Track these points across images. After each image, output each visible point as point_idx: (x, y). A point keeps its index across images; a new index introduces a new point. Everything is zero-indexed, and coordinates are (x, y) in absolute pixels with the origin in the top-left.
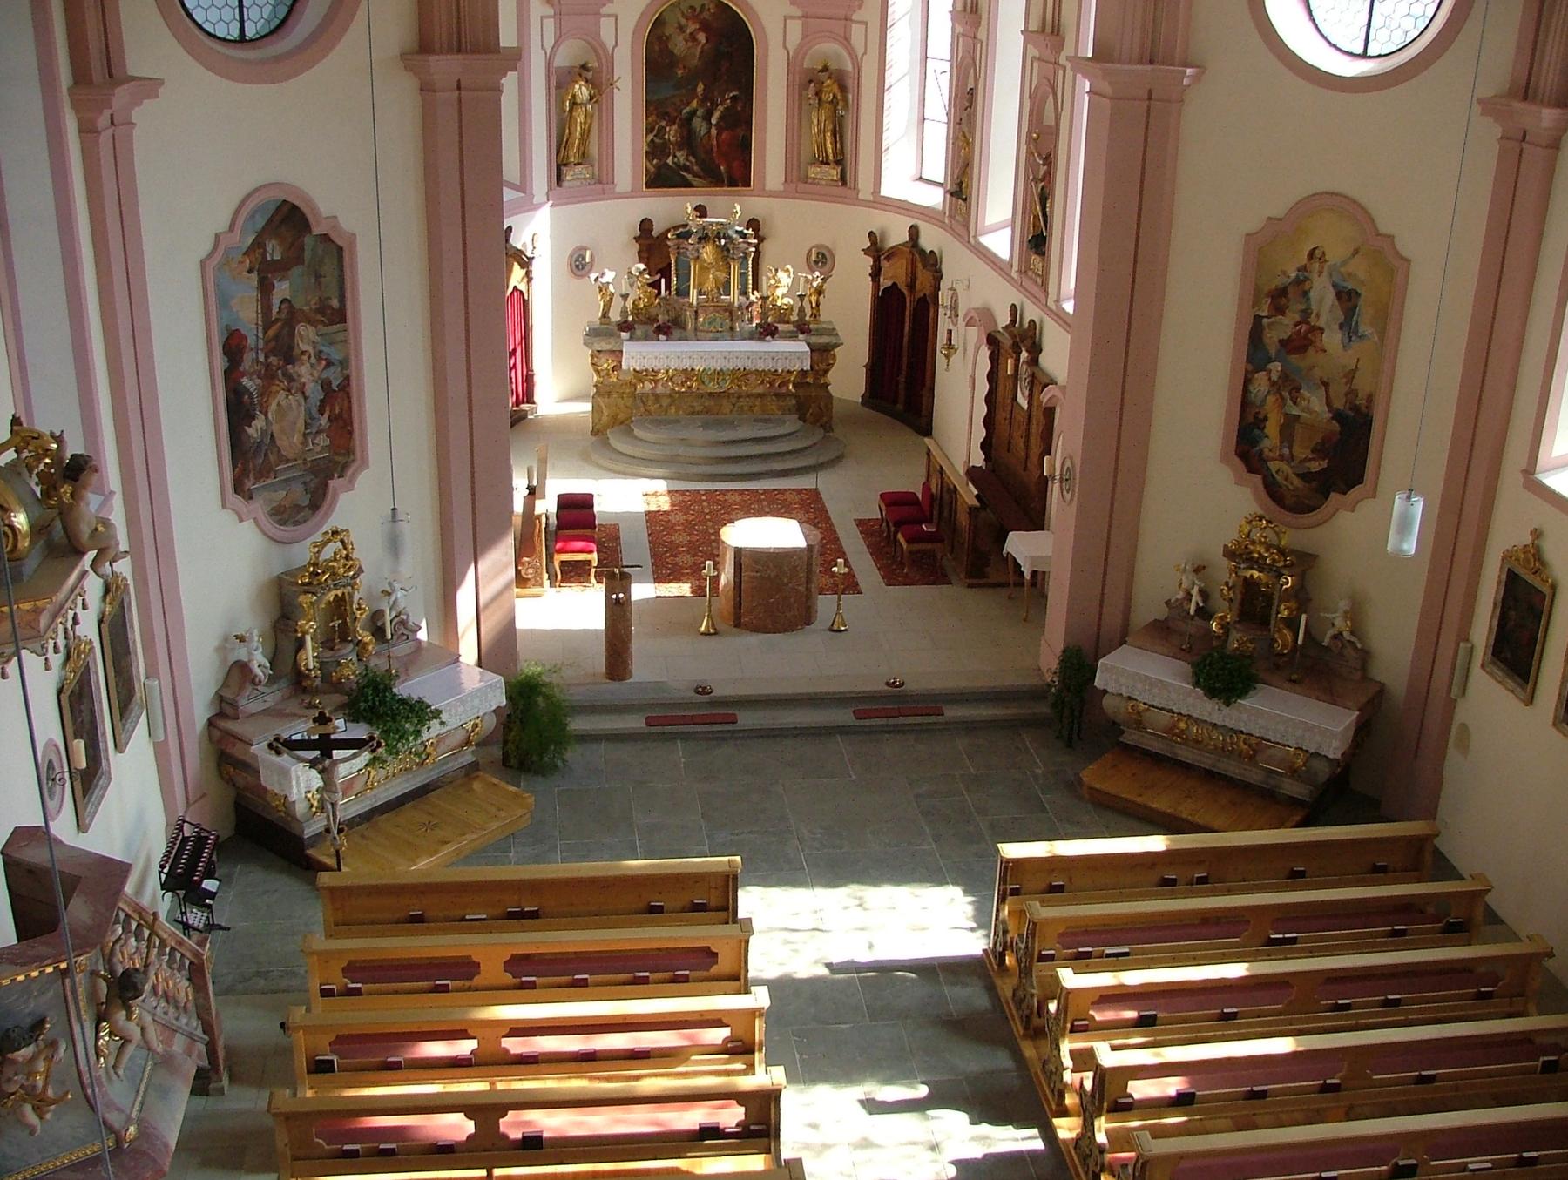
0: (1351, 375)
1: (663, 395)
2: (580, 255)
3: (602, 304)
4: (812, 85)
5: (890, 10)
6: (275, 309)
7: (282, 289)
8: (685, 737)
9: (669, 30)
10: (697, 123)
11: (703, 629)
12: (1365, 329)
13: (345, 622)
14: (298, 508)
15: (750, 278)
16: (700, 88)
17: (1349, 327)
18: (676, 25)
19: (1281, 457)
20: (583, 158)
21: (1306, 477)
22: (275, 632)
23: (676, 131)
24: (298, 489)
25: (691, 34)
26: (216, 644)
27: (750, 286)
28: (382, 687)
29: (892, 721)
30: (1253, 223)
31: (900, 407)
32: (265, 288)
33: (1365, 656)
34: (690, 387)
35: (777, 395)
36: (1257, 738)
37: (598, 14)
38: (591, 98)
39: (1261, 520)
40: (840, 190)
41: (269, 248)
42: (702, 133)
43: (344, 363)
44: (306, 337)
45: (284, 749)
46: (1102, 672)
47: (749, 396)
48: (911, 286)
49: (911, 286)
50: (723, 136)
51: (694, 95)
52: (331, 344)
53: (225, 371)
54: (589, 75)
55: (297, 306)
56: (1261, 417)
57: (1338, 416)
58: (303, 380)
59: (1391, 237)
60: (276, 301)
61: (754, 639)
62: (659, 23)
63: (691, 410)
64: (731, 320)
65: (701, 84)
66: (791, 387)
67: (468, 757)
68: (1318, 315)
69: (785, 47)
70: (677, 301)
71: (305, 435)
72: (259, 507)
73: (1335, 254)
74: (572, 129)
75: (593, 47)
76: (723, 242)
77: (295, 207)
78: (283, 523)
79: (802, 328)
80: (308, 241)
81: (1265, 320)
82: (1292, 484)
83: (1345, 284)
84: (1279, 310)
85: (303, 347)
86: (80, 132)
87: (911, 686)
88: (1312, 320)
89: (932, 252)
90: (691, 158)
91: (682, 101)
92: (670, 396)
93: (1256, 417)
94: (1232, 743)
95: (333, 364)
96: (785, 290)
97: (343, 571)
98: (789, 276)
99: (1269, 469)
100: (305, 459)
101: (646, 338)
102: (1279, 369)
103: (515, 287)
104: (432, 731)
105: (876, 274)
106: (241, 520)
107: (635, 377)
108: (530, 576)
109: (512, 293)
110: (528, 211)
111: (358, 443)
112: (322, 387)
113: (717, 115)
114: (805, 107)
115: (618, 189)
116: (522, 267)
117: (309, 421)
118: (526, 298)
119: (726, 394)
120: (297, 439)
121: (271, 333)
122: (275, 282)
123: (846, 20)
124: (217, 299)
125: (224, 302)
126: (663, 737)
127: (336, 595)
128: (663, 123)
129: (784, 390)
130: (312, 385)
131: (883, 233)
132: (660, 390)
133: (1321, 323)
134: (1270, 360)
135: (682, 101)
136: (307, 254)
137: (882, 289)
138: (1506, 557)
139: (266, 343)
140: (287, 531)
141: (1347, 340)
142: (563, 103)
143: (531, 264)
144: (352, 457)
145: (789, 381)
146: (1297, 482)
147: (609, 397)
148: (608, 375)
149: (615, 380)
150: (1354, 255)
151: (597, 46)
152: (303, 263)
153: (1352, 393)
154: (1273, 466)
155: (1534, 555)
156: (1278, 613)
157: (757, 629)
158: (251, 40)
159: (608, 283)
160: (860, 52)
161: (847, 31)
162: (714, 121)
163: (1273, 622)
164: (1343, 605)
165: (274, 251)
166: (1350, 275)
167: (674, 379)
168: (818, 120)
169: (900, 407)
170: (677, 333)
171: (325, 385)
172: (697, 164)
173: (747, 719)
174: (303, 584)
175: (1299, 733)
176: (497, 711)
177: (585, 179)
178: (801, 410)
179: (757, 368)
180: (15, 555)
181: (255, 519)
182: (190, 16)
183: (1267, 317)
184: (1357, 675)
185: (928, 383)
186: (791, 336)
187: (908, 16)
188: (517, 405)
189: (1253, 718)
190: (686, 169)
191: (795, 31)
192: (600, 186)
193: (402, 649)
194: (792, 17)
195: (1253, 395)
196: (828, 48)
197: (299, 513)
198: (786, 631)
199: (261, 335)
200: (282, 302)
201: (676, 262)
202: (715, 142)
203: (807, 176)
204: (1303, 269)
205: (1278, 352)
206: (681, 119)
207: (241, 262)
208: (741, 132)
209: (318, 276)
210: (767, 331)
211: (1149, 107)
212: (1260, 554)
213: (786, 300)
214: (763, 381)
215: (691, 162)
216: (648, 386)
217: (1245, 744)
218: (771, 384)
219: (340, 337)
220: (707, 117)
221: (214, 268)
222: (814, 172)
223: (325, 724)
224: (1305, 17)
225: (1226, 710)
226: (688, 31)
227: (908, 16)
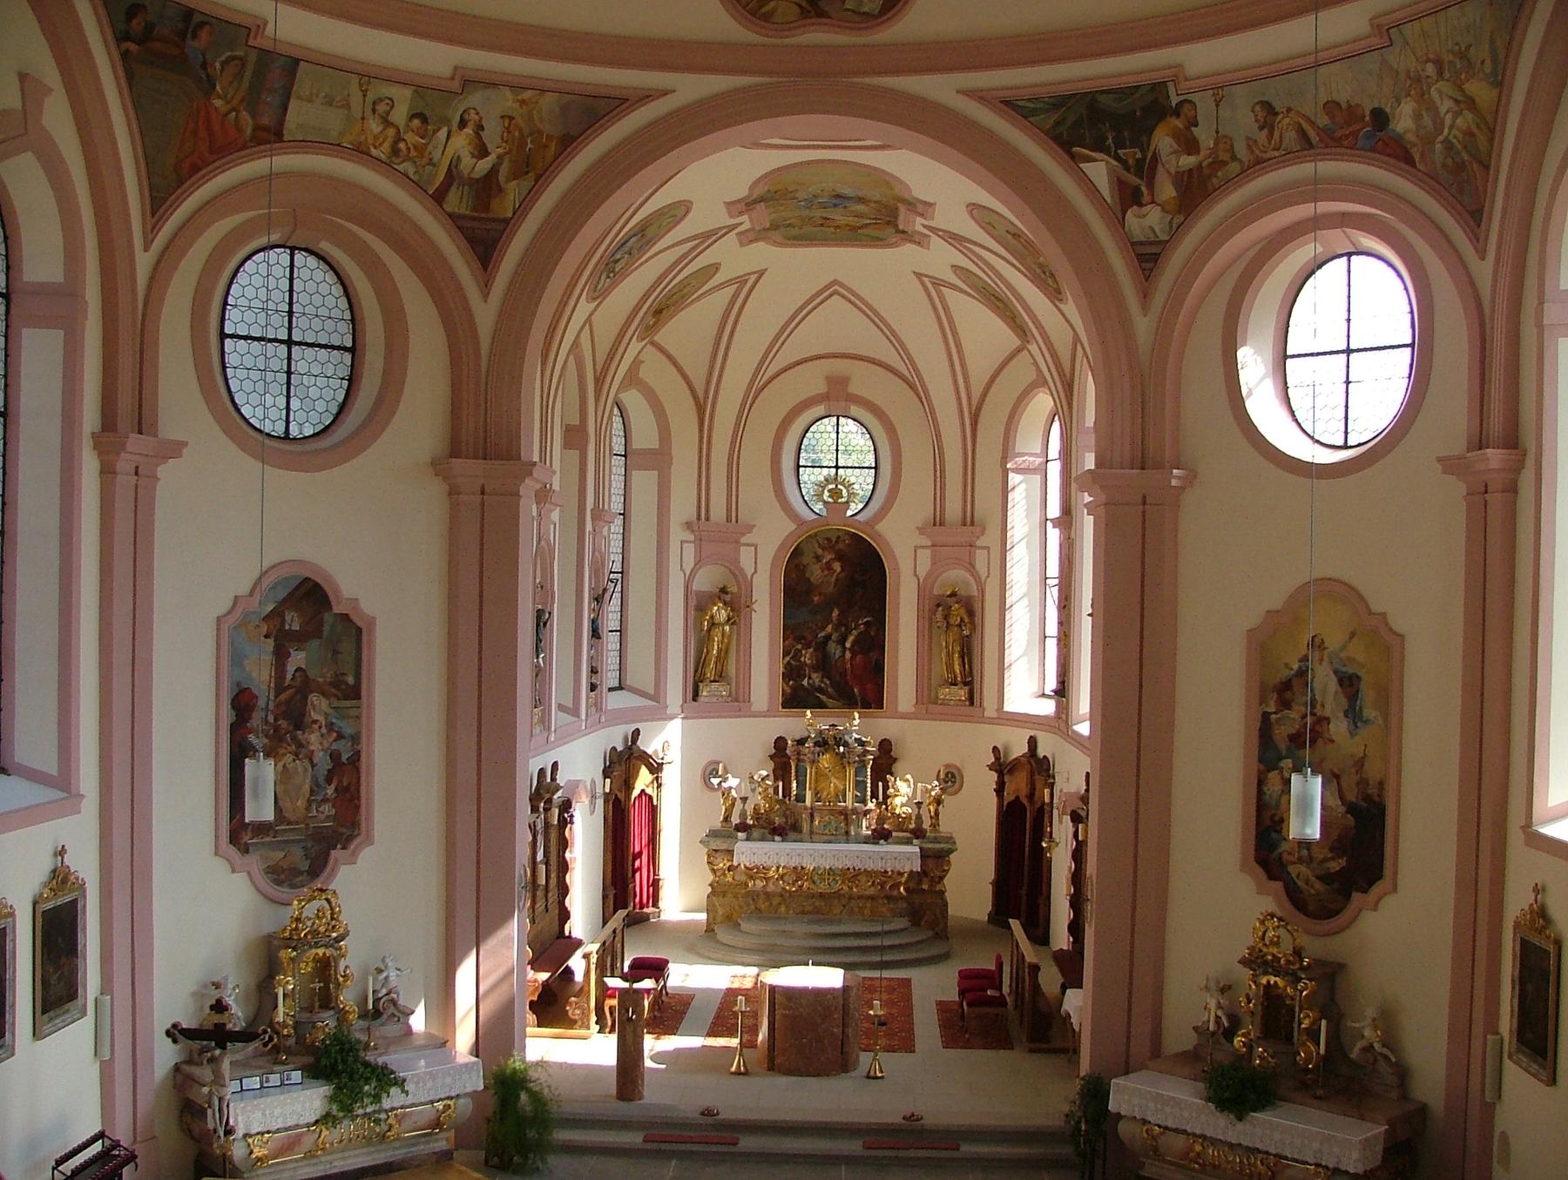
0: (1360, 764)
1: (774, 894)
2: (714, 769)
3: (724, 807)
4: (940, 609)
5: (1009, 534)
6: (289, 676)
7: (297, 659)
8: (681, 1155)
9: (807, 559)
10: (833, 648)
11: (733, 1069)
12: (1369, 713)
13: (327, 988)
14: (295, 872)
15: (869, 785)
16: (835, 613)
17: (1354, 714)
18: (812, 555)
19: (1301, 860)
20: (720, 677)
21: (1325, 878)
22: (260, 992)
24: (298, 852)
26: (194, 988)
27: (869, 793)
28: (347, 1046)
29: (901, 1153)
30: (1253, 619)
32: (281, 655)
33: (1403, 1074)
34: (801, 887)
35: (888, 898)
36: (1275, 1156)
38: (729, 620)
39: (1272, 918)
40: (968, 710)
41: (288, 618)
42: (837, 656)
43: (356, 739)
44: (319, 706)
45: (181, 1037)
46: (1115, 1093)
47: (860, 897)
48: (1031, 796)
49: (1031, 796)
50: (858, 659)
51: (828, 621)
52: (344, 717)
53: (231, 725)
54: (728, 598)
55: (311, 674)
56: (1277, 818)
57: (1351, 809)
58: (312, 748)
59: (1384, 615)
60: (291, 669)
61: (783, 1081)
62: (797, 553)
64: (847, 825)
66: (902, 889)
67: (441, 1143)
68: (1323, 706)
69: (916, 575)
70: (795, 806)
71: (309, 802)
72: (254, 861)
73: (1334, 640)
74: (710, 648)
75: (734, 574)
76: (842, 749)
77: (317, 585)
78: (279, 883)
79: (918, 833)
80: (328, 617)
81: (1273, 716)
82: (1312, 887)
83: (1344, 669)
84: (1285, 704)
85: (314, 716)
86: (101, 472)
87: (929, 1121)
88: (1318, 711)
89: (1045, 757)
90: (825, 680)
93: (1272, 818)
94: (1249, 1164)
95: (344, 737)
96: (905, 799)
97: (331, 936)
98: (909, 786)
99: (1289, 874)
100: (307, 824)
101: (763, 839)
102: (1291, 766)
103: (643, 791)
104: (393, 1099)
105: (1000, 791)
106: (233, 871)
107: (747, 874)
108: (577, 1017)
109: (640, 796)
110: (659, 719)
111: (363, 818)
112: (331, 758)
113: (851, 638)
114: (935, 630)
116: (651, 772)
117: (315, 788)
118: (655, 803)
120: (301, 803)
121: (283, 697)
122: (291, 650)
123: (971, 546)
124: (231, 654)
125: (237, 659)
126: (659, 1154)
127: (317, 954)
128: (799, 646)
129: (895, 893)
130: (321, 754)
131: (1006, 748)
132: (771, 887)
133: (1327, 713)
134: (1281, 758)
136: (327, 628)
137: (1005, 803)
138: (1517, 926)
139: (277, 706)
140: (282, 892)
141: (1353, 727)
142: (702, 623)
143: (661, 770)
144: (356, 833)
145: (899, 884)
146: (1318, 885)
147: (724, 896)
148: (724, 874)
149: (731, 880)
150: (1351, 638)
151: (737, 572)
152: (321, 638)
153: (1363, 783)
154: (1293, 870)
155: (1540, 916)
156: (1300, 1024)
157: (789, 1072)
158: (295, 439)
159: (730, 788)
160: (983, 574)
161: (971, 556)
162: (848, 645)
163: (1296, 1034)
164: (1370, 1012)
165: (293, 621)
166: (1349, 659)
167: (785, 878)
168: (946, 642)
170: (792, 835)
171: (335, 756)
172: (832, 687)
173: (748, 1143)
174: (285, 938)
175: (1316, 1145)
176: (474, 1095)
177: (722, 696)
178: (915, 916)
180: (228, 1128)
181: (249, 873)
182: (238, 410)
183: (1275, 713)
184: (1394, 1094)
186: (908, 842)
187: (1026, 540)
188: (641, 908)
189: (1268, 1132)
190: (820, 690)
191: (925, 557)
192: (736, 704)
193: (391, 1030)
195: (1267, 797)
196: (955, 576)
197: (297, 877)
198: (818, 1075)
199: (272, 697)
200: (296, 671)
201: (797, 766)
204: (1305, 659)
205: (1288, 749)
207: (258, 626)
208: (874, 655)
209: (336, 652)
210: (880, 835)
211: (1144, 512)
212: (1273, 955)
213: (904, 809)
214: (874, 882)
216: (760, 884)
217: (1262, 1164)
218: (882, 885)
219: (353, 712)
220: (842, 641)
221: (232, 629)
222: (945, 692)
223: (222, 1012)
224: (1288, 419)
225: (1240, 1126)
227: (1026, 540)
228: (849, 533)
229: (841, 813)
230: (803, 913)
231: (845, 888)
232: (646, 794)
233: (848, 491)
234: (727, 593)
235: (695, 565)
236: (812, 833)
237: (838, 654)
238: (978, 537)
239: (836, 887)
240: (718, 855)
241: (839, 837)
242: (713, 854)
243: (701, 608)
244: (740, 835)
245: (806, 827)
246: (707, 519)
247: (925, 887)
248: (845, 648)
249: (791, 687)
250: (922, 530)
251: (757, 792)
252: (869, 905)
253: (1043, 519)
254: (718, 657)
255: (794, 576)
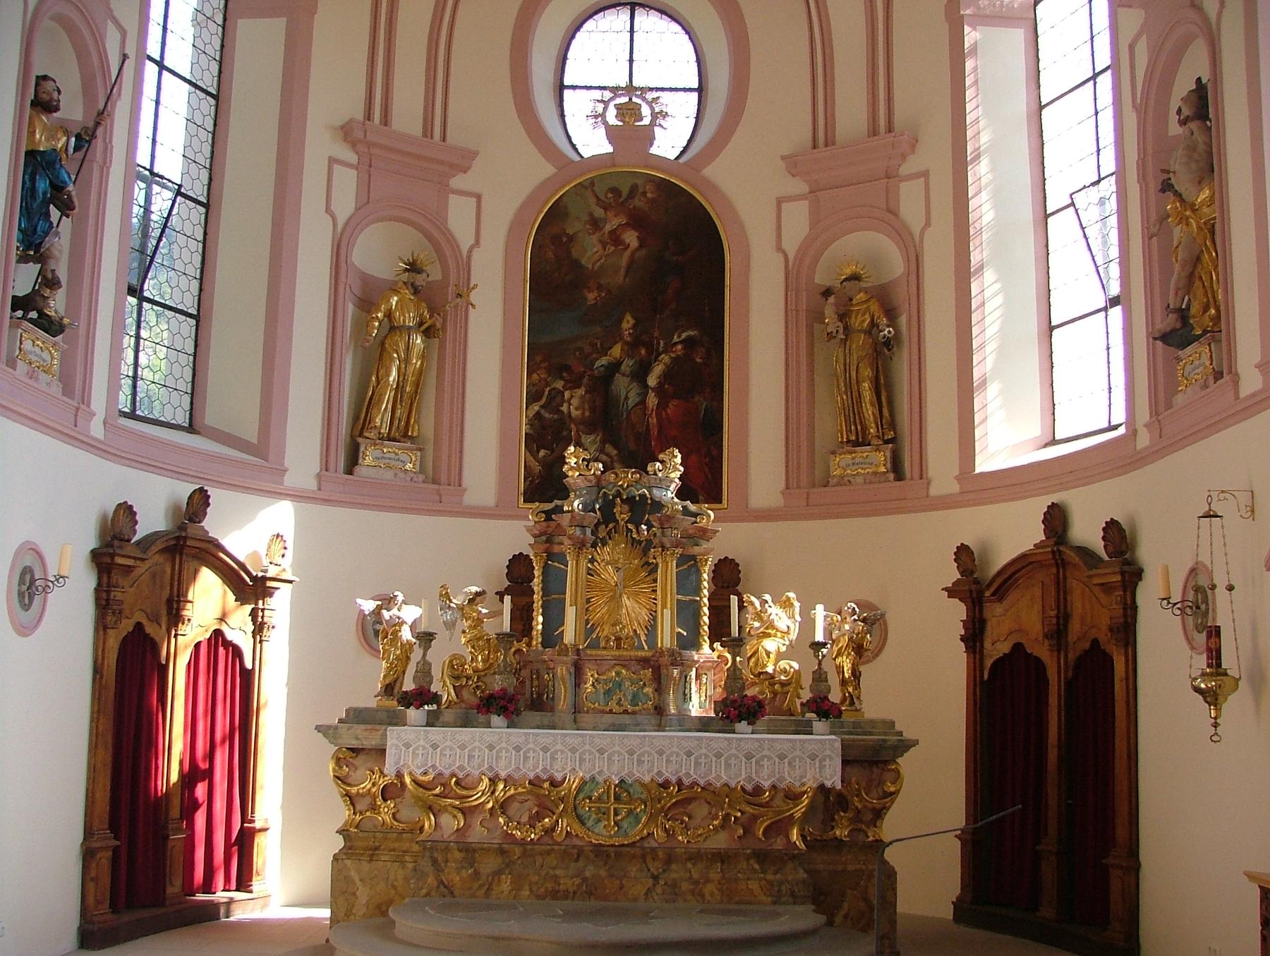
4: (832, 299)
9: (574, 226)
10: (623, 387)
16: (628, 323)
18: (586, 218)
20: (402, 434)
23: (582, 397)
25: (613, 232)
31: (1047, 912)
34: (550, 831)
35: (763, 857)
37: (445, 190)
38: (421, 324)
42: (631, 402)
47: (695, 857)
49: (1058, 633)
51: (613, 335)
54: (420, 280)
62: (556, 213)
63: (549, 886)
65: (628, 317)
69: (779, 248)
79: (821, 707)
91: (593, 345)
92: (502, 852)
105: (974, 636)
113: (658, 370)
115: (471, 499)
118: (249, 665)
119: (639, 852)
128: (559, 385)
129: (779, 843)
131: (985, 550)
132: (478, 834)
135: (593, 345)
137: (988, 663)
148: (374, 808)
149: (388, 819)
160: (915, 223)
162: (652, 381)
169: (1047, 912)
179: (711, 778)
185: (1121, 833)
191: (797, 222)
192: (437, 486)
194: (790, 199)
202: (653, 420)
203: (828, 475)
206: (592, 377)
208: (702, 402)
213: (783, 664)
215: (610, 457)
216: (451, 823)
220: (640, 374)
222: (842, 464)
226: (608, 228)
228: (652, 179)
229: (644, 662)
230: (555, 895)
231: (659, 834)
232: (228, 644)
233: (652, 109)
234: (419, 271)
235: (358, 209)
236: (577, 709)
237: (633, 399)
238: (904, 157)
239: (635, 832)
240: (359, 761)
241: (639, 717)
242: (349, 757)
243: (366, 304)
244: (412, 713)
245: (563, 697)
246: (386, 120)
247: (841, 832)
248: (646, 386)
249: (543, 462)
250: (793, 164)
251: (459, 628)
252: (715, 875)
253: (1035, 107)
254: (399, 388)
255: (550, 254)
